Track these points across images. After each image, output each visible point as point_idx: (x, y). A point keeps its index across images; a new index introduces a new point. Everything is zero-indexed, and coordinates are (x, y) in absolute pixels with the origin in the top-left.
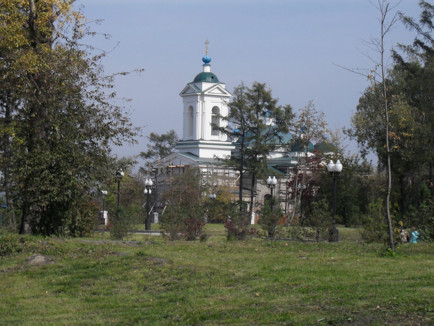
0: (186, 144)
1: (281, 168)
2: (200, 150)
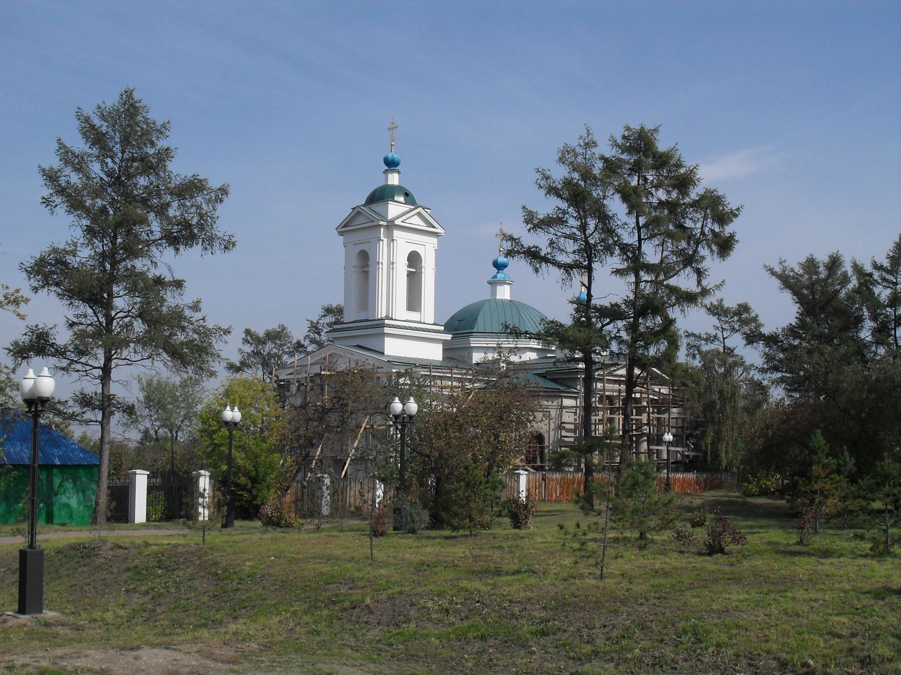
0: (351, 329)
1: (557, 377)
2: (387, 339)
